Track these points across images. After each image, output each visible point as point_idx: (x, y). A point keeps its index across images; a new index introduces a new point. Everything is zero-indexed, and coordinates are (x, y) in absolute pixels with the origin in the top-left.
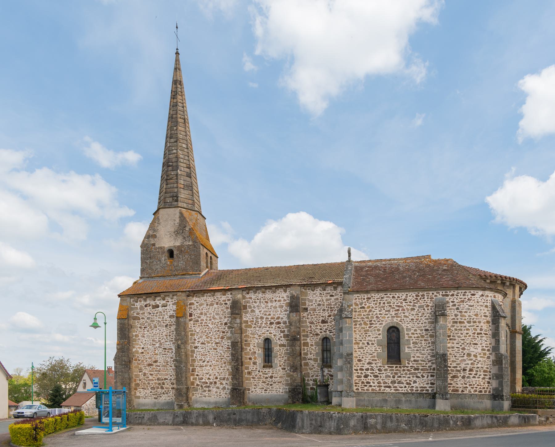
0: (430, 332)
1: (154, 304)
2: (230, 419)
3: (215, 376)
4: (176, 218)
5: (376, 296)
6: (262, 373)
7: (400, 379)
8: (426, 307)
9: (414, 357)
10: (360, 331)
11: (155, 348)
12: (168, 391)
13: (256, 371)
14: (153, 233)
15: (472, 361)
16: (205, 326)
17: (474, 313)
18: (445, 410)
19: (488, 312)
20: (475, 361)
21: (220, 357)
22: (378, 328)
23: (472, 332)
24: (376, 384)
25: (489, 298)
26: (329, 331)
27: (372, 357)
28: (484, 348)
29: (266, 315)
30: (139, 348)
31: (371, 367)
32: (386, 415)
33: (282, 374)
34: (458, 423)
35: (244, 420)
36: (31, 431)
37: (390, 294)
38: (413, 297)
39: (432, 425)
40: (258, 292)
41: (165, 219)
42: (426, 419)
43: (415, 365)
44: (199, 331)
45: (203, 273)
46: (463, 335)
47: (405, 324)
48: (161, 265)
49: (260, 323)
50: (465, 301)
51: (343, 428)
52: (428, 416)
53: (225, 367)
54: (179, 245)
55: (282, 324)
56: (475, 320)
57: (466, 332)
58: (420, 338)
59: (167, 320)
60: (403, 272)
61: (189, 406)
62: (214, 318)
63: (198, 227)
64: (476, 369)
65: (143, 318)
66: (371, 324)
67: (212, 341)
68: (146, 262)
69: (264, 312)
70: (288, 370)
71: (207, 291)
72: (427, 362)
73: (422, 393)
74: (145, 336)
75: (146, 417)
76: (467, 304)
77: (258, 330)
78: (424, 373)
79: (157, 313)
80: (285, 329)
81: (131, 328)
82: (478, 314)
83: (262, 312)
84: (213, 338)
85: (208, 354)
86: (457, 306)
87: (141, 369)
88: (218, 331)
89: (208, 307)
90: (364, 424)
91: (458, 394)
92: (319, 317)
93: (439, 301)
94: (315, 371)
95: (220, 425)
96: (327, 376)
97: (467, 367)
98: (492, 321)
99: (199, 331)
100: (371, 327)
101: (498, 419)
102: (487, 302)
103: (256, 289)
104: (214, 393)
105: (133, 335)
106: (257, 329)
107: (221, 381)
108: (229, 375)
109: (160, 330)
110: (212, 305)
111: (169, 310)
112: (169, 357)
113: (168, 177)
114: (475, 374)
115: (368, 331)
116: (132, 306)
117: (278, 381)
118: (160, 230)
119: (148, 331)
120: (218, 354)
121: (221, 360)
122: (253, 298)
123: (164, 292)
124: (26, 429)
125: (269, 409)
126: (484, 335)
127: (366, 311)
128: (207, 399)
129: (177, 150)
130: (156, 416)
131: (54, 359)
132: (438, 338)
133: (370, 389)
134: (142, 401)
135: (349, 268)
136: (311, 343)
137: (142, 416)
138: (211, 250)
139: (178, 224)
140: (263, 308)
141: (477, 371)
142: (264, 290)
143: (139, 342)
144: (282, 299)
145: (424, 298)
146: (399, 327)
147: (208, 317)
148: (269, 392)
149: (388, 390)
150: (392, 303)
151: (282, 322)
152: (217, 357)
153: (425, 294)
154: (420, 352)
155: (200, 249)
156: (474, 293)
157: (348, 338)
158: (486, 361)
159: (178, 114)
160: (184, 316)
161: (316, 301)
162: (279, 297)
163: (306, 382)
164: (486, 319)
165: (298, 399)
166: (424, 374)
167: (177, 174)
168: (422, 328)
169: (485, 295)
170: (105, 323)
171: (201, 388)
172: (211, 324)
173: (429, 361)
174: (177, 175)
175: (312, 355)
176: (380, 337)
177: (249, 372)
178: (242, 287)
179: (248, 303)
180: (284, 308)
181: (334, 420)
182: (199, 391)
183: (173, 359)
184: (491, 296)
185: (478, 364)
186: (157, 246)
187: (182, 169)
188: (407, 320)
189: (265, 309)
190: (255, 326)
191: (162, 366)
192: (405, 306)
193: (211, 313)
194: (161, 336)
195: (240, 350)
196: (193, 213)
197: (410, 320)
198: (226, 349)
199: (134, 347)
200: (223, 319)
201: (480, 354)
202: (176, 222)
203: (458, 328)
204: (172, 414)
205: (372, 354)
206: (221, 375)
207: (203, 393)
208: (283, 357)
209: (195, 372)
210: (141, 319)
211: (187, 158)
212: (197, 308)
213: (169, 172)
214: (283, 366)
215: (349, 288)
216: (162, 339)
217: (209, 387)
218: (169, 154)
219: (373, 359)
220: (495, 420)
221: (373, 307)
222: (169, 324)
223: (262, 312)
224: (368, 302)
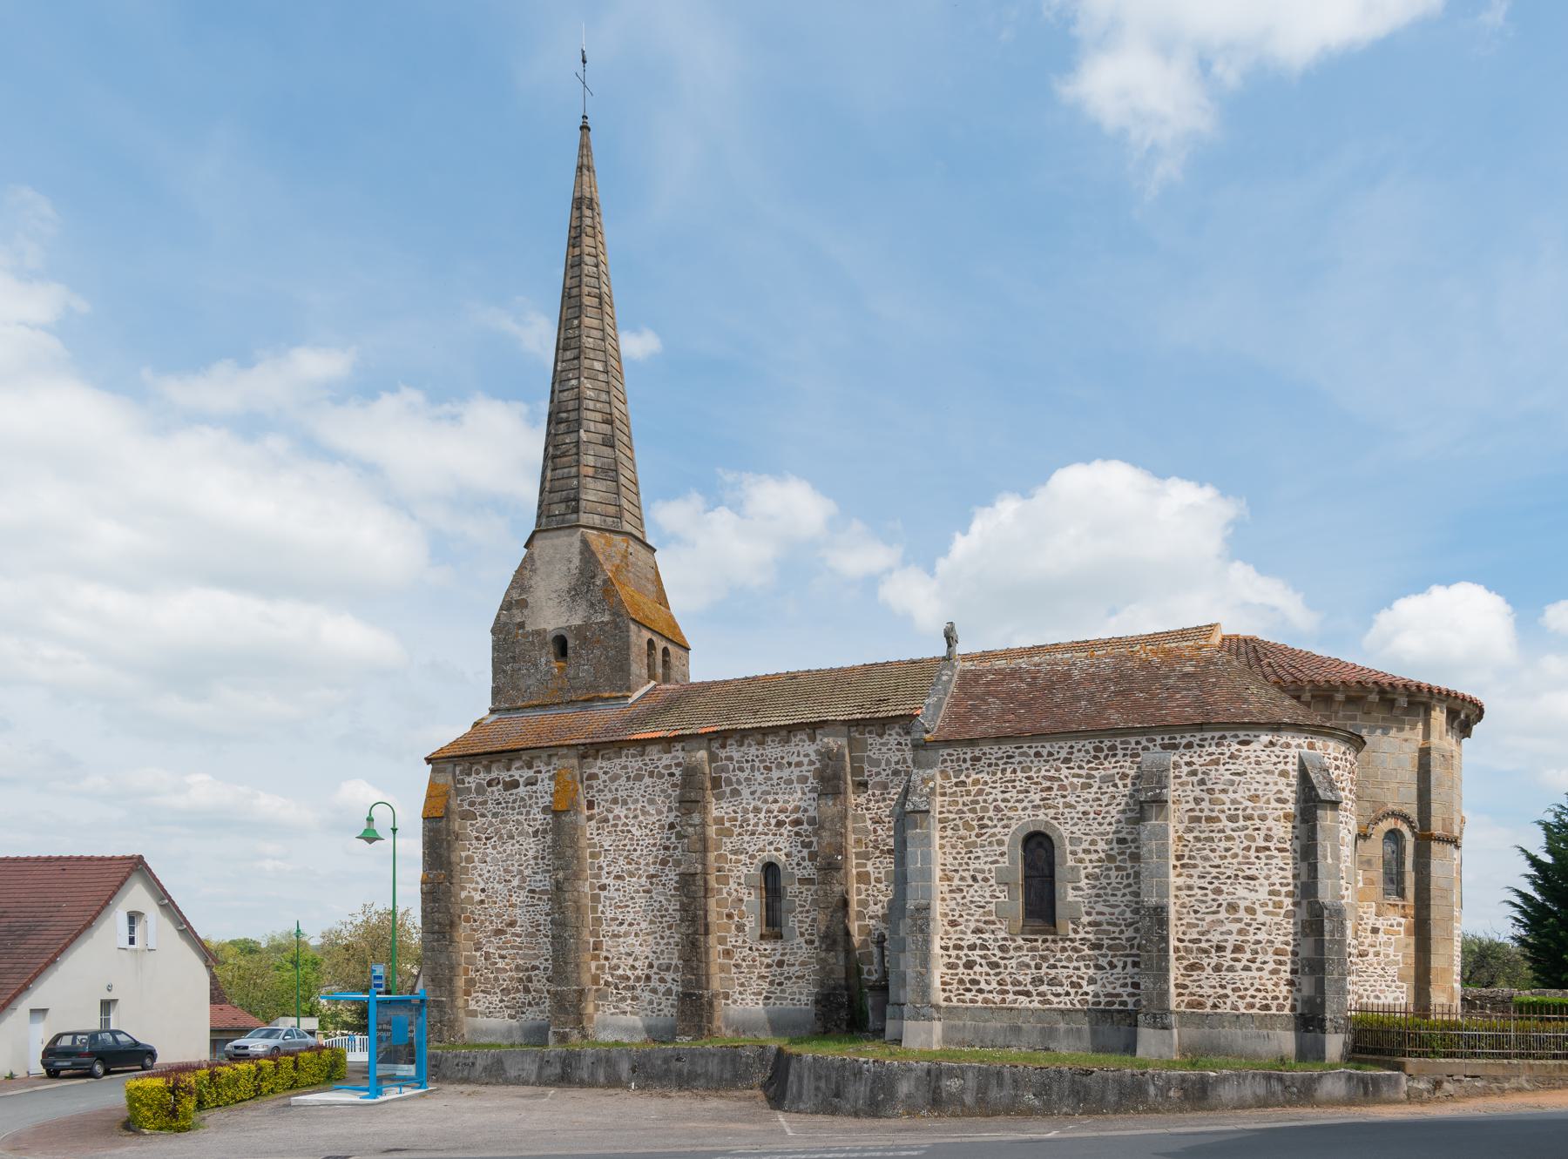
0: (1130, 847)
6: (756, 954)
7: (1053, 972)
8: (1121, 779)
9: (1089, 914)
10: (953, 847)
12: (541, 998)
15: (1241, 925)
16: (622, 832)
17: (1248, 793)
18: (1161, 1057)
19: (1290, 789)
20: (1250, 925)
21: (658, 911)
22: (999, 837)
23: (1242, 846)
24: (994, 985)
25: (1293, 751)
28: (1277, 887)
30: (475, 890)
31: (980, 941)
32: (987, 1070)
33: (806, 955)
34: (1171, 1093)
35: (700, 1075)
36: (164, 1096)
37: (1030, 747)
38: (1087, 752)
39: (1103, 1098)
40: (746, 742)
42: (1086, 1080)
45: (636, 695)
46: (1217, 854)
47: (1068, 826)
49: (752, 822)
50: (1222, 761)
51: (883, 1100)
52: (1093, 1072)
53: (669, 938)
55: (805, 826)
56: (1249, 811)
57: (1224, 844)
58: (1106, 863)
60: (1079, 683)
61: (585, 1037)
64: (1254, 947)
65: (483, 815)
66: (982, 827)
67: (640, 872)
68: (504, 671)
72: (1123, 927)
73: (1109, 1011)
74: (488, 859)
75: (480, 1063)
76: (1227, 770)
77: (748, 842)
78: (1115, 956)
81: (457, 839)
82: (1257, 796)
85: (632, 906)
86: (1200, 776)
88: (654, 845)
89: (632, 782)
90: (934, 1092)
91: (1202, 1015)
93: (1153, 762)
95: (646, 1086)
97: (1226, 941)
98: (1301, 814)
100: (982, 835)
101: (1287, 1083)
102: (1286, 763)
103: (742, 735)
104: (645, 1004)
105: (461, 857)
106: (747, 838)
110: (639, 778)
112: (543, 913)
113: (557, 450)
114: (1248, 961)
115: (974, 844)
118: (535, 586)
119: (494, 847)
122: (736, 759)
123: (527, 749)
124: (153, 1090)
125: (761, 1047)
126: (1275, 853)
127: (968, 793)
129: (579, 378)
130: (502, 1063)
131: (373, 910)
132: (1145, 863)
133: (980, 997)
134: (481, 1022)
135: (945, 678)
136: (876, 875)
137: (471, 1060)
138: (666, 633)
140: (760, 784)
141: (1257, 953)
142: (759, 737)
143: (473, 874)
144: (806, 760)
146: (1051, 834)
148: (775, 1004)
150: (1034, 769)
151: (805, 819)
152: (653, 911)
153: (1117, 744)
154: (1105, 901)
155: (628, 631)
156: (1247, 738)
157: (919, 865)
158: (1283, 922)
159: (583, 286)
160: (573, 807)
161: (888, 762)
162: (798, 756)
163: (866, 976)
164: (1282, 809)
167: (578, 442)
169: (1279, 743)
170: (394, 830)
171: (615, 991)
173: (1128, 925)
174: (577, 443)
175: (880, 905)
178: (707, 730)
179: (723, 771)
184: (1299, 746)
185: (1259, 932)
186: (529, 628)
187: (592, 426)
188: (1071, 815)
189: (764, 788)
191: (526, 936)
192: (1066, 777)
195: (702, 894)
196: (618, 538)
197: (1080, 815)
198: (673, 892)
199: (463, 888)
201: (1264, 905)
202: (573, 566)
203: (1203, 836)
205: (983, 907)
207: (620, 1005)
208: (808, 912)
209: (602, 950)
211: (604, 397)
212: (606, 786)
214: (809, 934)
215: (927, 732)
216: (527, 868)
217: (634, 988)
218: (560, 392)
219: (987, 918)
220: (1277, 1087)
221: (986, 783)
223: (758, 794)
224: (974, 769)
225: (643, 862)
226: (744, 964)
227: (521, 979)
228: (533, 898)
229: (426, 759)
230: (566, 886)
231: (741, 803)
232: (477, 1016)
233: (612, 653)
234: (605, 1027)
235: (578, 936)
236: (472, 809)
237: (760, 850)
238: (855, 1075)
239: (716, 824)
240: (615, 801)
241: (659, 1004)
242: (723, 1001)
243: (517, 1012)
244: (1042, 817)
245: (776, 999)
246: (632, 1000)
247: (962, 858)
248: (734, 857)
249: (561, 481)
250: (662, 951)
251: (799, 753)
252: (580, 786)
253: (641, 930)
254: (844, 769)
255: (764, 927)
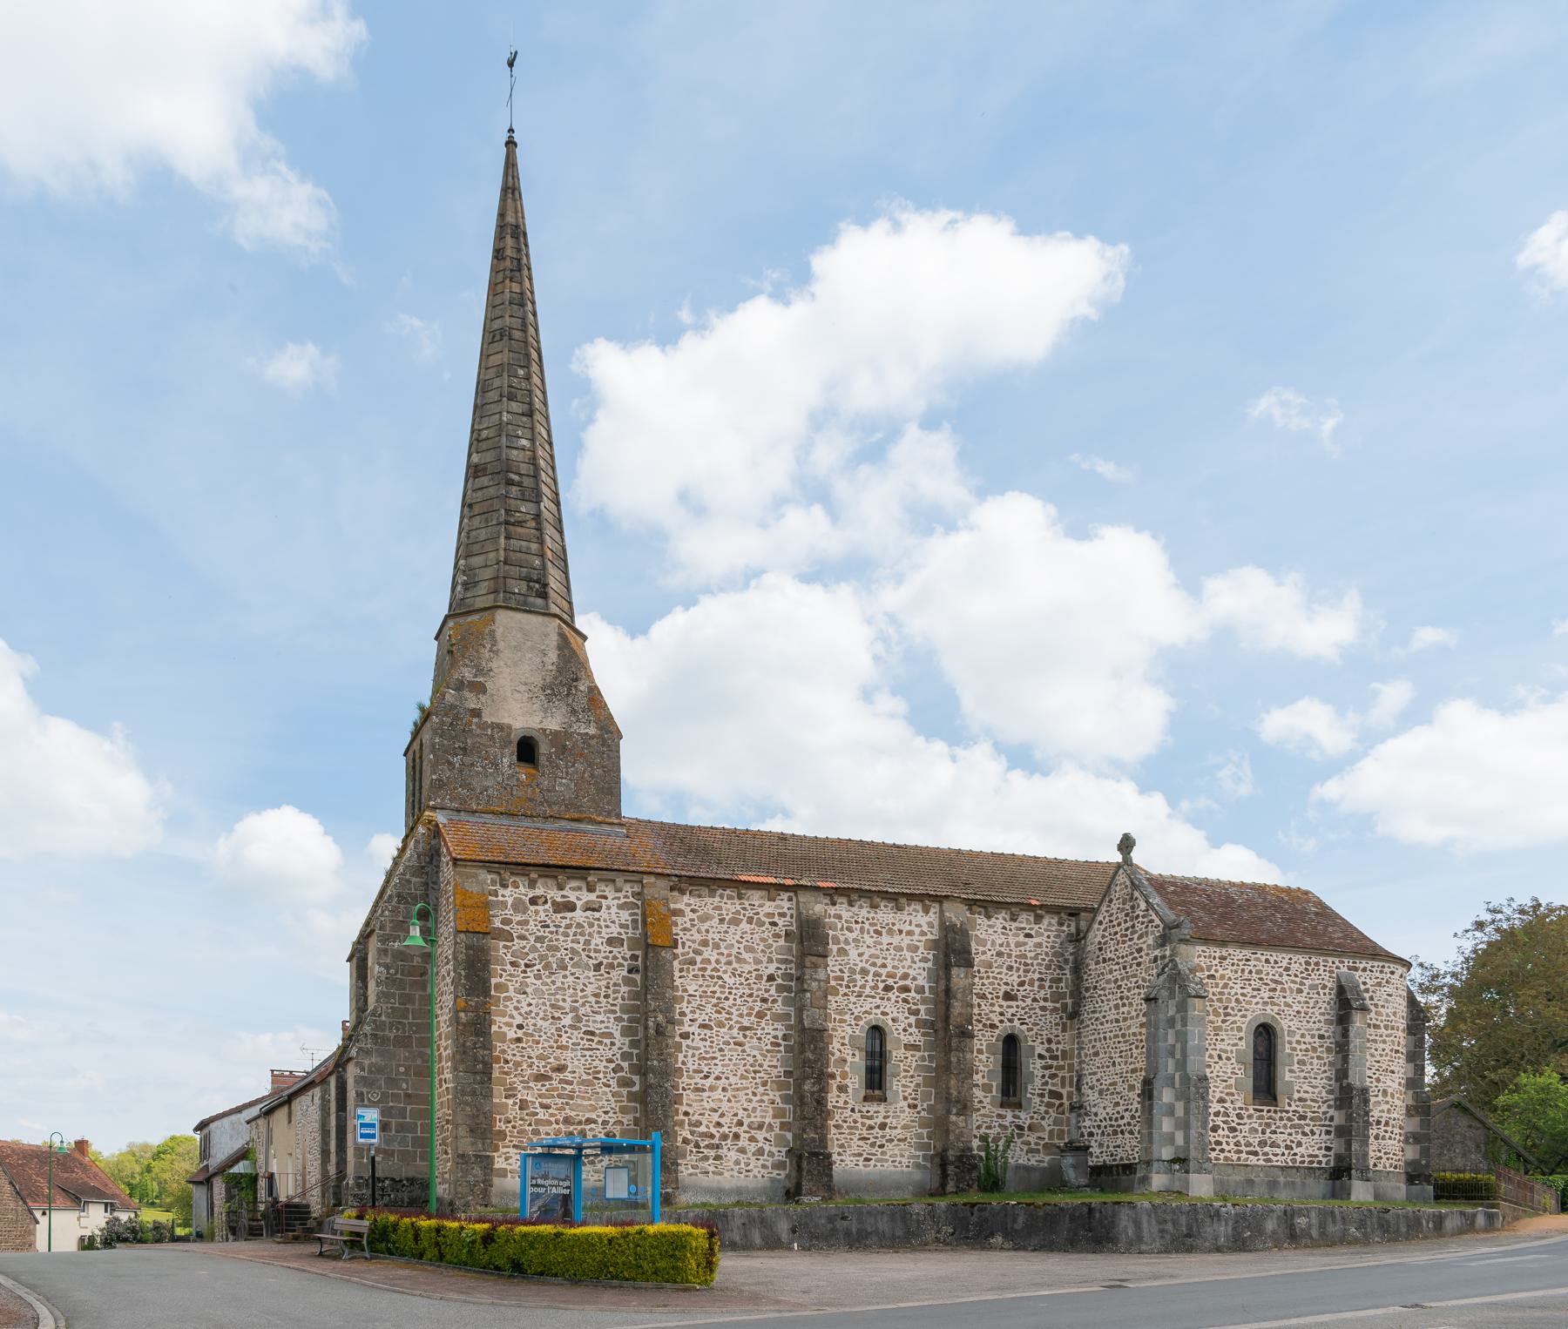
2: (833, 1230)
3: (736, 1119)
4: (547, 646)
5: (1237, 953)
7: (1273, 1136)
9: (1299, 1091)
11: (558, 1029)
14: (475, 676)
21: (751, 1065)
22: (1239, 1024)
24: (1232, 1146)
26: (1019, 1019)
27: (1226, 1087)
29: (874, 964)
30: (509, 1025)
35: (871, 1233)
38: (1300, 964)
41: (514, 643)
42: (1387, 1216)
43: (1300, 1109)
44: (696, 991)
48: (500, 779)
49: (859, 984)
51: (1250, 1237)
55: (913, 994)
59: (599, 951)
62: (739, 960)
65: (522, 937)
66: (1227, 1014)
68: (449, 763)
69: (870, 956)
70: (923, 1109)
74: (529, 990)
77: (854, 1003)
79: (569, 926)
80: (919, 1007)
83: (865, 957)
84: (736, 1013)
86: (1371, 994)
87: (510, 1089)
88: (751, 995)
89: (725, 926)
92: (999, 984)
94: (984, 1115)
96: (1010, 1129)
97: (1382, 1117)
99: (696, 991)
104: (731, 1164)
106: (853, 999)
108: (774, 1117)
109: (578, 978)
110: (735, 922)
111: (605, 921)
112: (604, 1059)
115: (1220, 1028)
116: (490, 898)
118: (496, 671)
119: (538, 977)
120: (748, 1058)
127: (1217, 985)
128: (712, 1181)
133: (1222, 1156)
136: (979, 1047)
140: (868, 947)
143: (507, 1006)
144: (917, 930)
145: (1318, 970)
147: (723, 954)
148: (875, 1166)
149: (1253, 1160)
151: (913, 986)
152: (745, 1065)
154: (1310, 1082)
161: (993, 943)
162: (910, 924)
166: (1315, 1129)
168: (1314, 1032)
171: (694, 1150)
172: (729, 974)
176: (1242, 1045)
180: (920, 951)
181: (1226, 1221)
182: (688, 1158)
183: (613, 1065)
189: (873, 951)
190: (847, 990)
191: (578, 1084)
193: (733, 945)
194: (580, 994)
198: (769, 1047)
200: (765, 965)
205: (1226, 1081)
206: (753, 1115)
207: (700, 1164)
208: (912, 1077)
210: (516, 940)
213: (512, 501)
214: (912, 1099)
216: (583, 1005)
217: (718, 1147)
221: (1230, 979)
222: (605, 961)
223: (865, 957)
228: (592, 1041)
232: (506, 1176)
244: (1269, 1011)
245: (877, 1161)
247: (1211, 1039)
251: (911, 922)
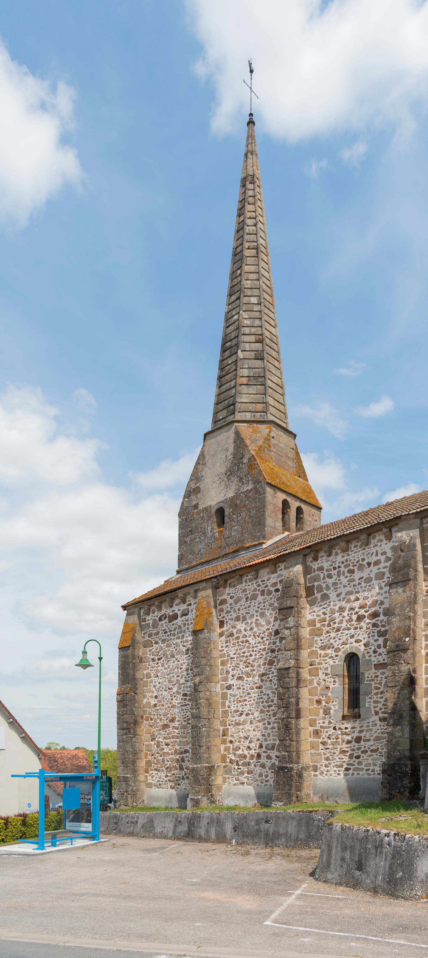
1: (171, 614)
2: (259, 831)
6: (339, 732)
13: (329, 727)
14: (196, 484)
21: (267, 702)
30: (151, 697)
33: (379, 731)
35: (281, 835)
40: (334, 552)
41: (213, 453)
45: (269, 543)
51: (401, 878)
54: (232, 495)
55: (382, 617)
61: (213, 802)
63: (272, 453)
65: (156, 643)
68: (186, 542)
69: (346, 595)
71: (243, 571)
74: (159, 674)
75: (141, 822)
77: (334, 638)
85: (248, 700)
88: (264, 649)
89: (249, 602)
95: (243, 842)
104: (257, 776)
105: (144, 674)
106: (333, 635)
107: (268, 751)
111: (191, 620)
113: (223, 371)
116: (143, 623)
117: (372, 748)
118: (204, 475)
120: (264, 697)
121: (268, 709)
122: (325, 568)
125: (330, 812)
130: (153, 821)
134: (155, 791)
137: (135, 819)
138: (300, 495)
139: (232, 456)
140: (344, 586)
144: (383, 558)
148: (353, 774)
152: (263, 702)
160: (208, 625)
165: (402, 789)
170: (100, 659)
171: (236, 767)
172: (252, 637)
177: (316, 730)
179: (315, 580)
180: (386, 577)
186: (201, 507)
189: (348, 589)
191: (181, 728)
195: (294, 684)
196: (262, 427)
199: (145, 697)
202: (229, 453)
204: (173, 817)
206: (268, 739)
208: (382, 693)
209: (228, 736)
210: (154, 645)
212: (231, 608)
213: (226, 361)
214: (382, 713)
216: (182, 678)
217: (249, 764)
223: (343, 596)
225: (256, 664)
226: (329, 741)
227: (178, 760)
229: (122, 607)
230: (201, 688)
231: (329, 605)
233: (253, 512)
234: (229, 795)
235: (210, 726)
236: (150, 639)
237: (344, 643)
238: (376, 848)
239: (309, 626)
240: (238, 619)
241: (267, 776)
242: (313, 773)
243: (176, 784)
246: (248, 773)
248: (323, 652)
249: (225, 394)
250: (269, 734)
252: (214, 610)
253: (254, 719)
254: (414, 557)
255: (346, 709)
